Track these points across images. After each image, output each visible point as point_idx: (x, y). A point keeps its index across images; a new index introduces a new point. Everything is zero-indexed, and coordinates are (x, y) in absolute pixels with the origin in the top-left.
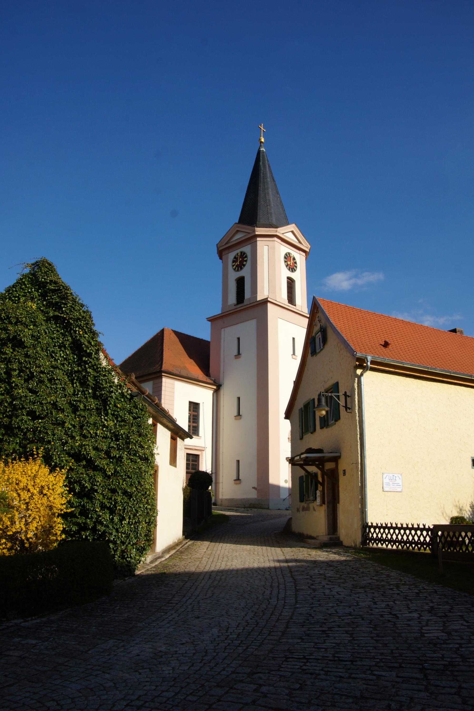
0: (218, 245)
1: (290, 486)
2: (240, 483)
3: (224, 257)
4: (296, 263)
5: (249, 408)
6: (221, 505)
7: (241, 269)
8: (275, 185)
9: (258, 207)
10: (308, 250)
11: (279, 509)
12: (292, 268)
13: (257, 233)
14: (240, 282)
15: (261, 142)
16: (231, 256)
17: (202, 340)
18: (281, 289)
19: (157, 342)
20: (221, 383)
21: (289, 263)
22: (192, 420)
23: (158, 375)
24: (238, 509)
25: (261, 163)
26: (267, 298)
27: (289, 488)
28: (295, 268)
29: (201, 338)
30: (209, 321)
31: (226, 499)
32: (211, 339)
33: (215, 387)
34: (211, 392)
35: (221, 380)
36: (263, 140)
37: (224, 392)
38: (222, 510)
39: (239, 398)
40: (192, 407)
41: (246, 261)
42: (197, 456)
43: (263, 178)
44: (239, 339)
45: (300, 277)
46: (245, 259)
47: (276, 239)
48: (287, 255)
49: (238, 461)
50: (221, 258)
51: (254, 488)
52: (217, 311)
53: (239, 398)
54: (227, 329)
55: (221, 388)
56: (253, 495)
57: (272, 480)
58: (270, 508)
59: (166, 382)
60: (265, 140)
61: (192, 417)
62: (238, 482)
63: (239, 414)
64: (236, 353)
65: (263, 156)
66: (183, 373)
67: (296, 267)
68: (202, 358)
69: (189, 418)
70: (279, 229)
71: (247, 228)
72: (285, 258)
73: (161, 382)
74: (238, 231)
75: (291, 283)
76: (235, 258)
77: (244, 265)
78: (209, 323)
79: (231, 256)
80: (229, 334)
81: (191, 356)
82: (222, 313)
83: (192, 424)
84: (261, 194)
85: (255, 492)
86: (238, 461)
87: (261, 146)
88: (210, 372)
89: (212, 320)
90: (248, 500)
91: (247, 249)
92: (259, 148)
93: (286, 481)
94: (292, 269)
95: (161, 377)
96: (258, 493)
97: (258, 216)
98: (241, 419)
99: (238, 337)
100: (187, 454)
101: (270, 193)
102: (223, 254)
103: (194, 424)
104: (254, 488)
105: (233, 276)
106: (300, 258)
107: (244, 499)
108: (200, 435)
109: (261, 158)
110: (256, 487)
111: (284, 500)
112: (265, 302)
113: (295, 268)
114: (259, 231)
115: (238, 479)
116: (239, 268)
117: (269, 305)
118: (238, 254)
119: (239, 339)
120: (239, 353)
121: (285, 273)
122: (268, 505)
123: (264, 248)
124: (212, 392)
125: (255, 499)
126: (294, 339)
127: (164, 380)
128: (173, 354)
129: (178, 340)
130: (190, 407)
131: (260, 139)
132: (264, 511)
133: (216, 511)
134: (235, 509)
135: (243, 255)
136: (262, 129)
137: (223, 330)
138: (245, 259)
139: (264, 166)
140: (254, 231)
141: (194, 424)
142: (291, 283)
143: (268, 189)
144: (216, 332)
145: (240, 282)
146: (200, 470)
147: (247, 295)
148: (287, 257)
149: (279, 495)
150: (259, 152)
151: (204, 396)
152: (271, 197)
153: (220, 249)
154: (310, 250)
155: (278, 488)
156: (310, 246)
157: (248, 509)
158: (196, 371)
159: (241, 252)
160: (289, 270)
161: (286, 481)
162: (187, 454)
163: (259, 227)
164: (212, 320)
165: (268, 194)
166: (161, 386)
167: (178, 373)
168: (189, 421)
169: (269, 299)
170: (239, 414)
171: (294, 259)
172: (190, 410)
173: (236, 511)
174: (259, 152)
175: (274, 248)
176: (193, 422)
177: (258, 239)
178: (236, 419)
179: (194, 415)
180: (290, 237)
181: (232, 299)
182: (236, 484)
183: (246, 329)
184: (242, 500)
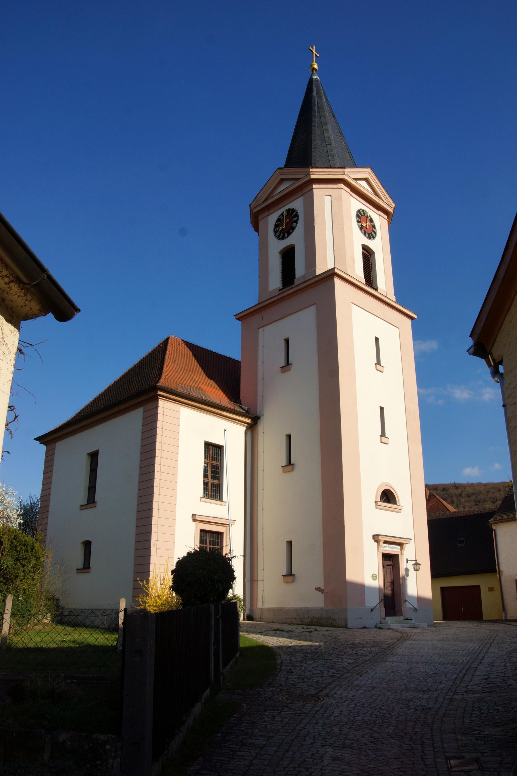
0: (252, 206)
1: (382, 585)
2: (293, 581)
3: (261, 224)
4: (374, 226)
5: (308, 453)
6: (261, 620)
7: (289, 234)
8: (337, 123)
9: (313, 147)
10: (391, 211)
11: (364, 628)
12: (370, 234)
13: (312, 176)
14: (288, 256)
15: (314, 69)
16: (273, 219)
17: (230, 358)
18: (353, 261)
19: (156, 359)
20: (258, 414)
21: (364, 224)
22: (210, 474)
23: (152, 394)
24: (290, 628)
25: (314, 94)
26: (334, 269)
27: (380, 589)
28: (373, 233)
29: (228, 355)
30: (238, 319)
31: (269, 609)
32: (242, 356)
33: (249, 421)
34: (242, 429)
35: (259, 409)
36: (316, 66)
37: (263, 428)
38: (261, 633)
39: (289, 437)
40: (210, 453)
41: (296, 222)
42: (220, 535)
43: (319, 111)
44: (287, 341)
45: (381, 246)
46: (294, 219)
47: (342, 185)
48: (360, 213)
49: (290, 543)
50: (257, 229)
51: (318, 589)
52: (251, 301)
53: (289, 437)
54: (267, 329)
55: (259, 422)
56: (317, 602)
57: (351, 575)
58: (349, 625)
59: (166, 408)
60: (318, 66)
61: (210, 469)
62: (290, 578)
63: (289, 462)
64: (283, 363)
65: (317, 85)
66: (195, 394)
67: (375, 233)
68: (229, 383)
69: (206, 470)
70: (347, 170)
71: (296, 172)
72: (357, 216)
73: (157, 407)
74: (282, 180)
75: (368, 256)
76: (279, 220)
77: (293, 229)
78: (240, 323)
79: (273, 219)
80: (271, 337)
81: (210, 375)
82: (258, 304)
83: (210, 481)
84: (316, 131)
85: (320, 596)
86: (290, 543)
87: (313, 73)
88: (241, 398)
89: (242, 317)
90: (308, 610)
91: (297, 204)
92: (311, 76)
93: (374, 577)
94: (369, 234)
95: (155, 399)
96: (325, 597)
97: (313, 158)
98: (292, 470)
99: (285, 337)
100: (202, 531)
101: (330, 130)
102: (260, 218)
103: (214, 481)
104: (318, 589)
105: (276, 246)
106: (380, 222)
107: (301, 609)
108: (225, 498)
109: (314, 88)
110: (322, 587)
111: (372, 610)
112: (331, 275)
113: (373, 233)
114: (316, 173)
115: (290, 575)
116: (286, 234)
117: (337, 280)
118: (284, 214)
119: (287, 341)
120: (288, 363)
121: (359, 239)
122: (346, 620)
123: (323, 198)
124: (244, 429)
125: (322, 609)
126: (377, 339)
127: (161, 403)
128: (179, 369)
129: (190, 353)
130: (206, 452)
131: (312, 65)
132: (338, 632)
133: (249, 638)
134: (286, 627)
135: (292, 214)
136: (314, 52)
137: (261, 330)
138: (294, 219)
139: (320, 97)
140: (309, 174)
141: (214, 481)
142: (368, 256)
143: (326, 124)
144: (250, 344)
145: (288, 256)
146: (45, 447)
147: (300, 271)
148: (361, 215)
149: (363, 602)
150: (311, 81)
151: (231, 434)
152: (331, 133)
153: (255, 211)
154: (394, 211)
155: (360, 588)
156: (394, 205)
157: (312, 628)
158: (217, 395)
159: (288, 211)
160: (365, 235)
161: (374, 577)
162: (202, 531)
163: (316, 167)
164: (242, 317)
165: (327, 130)
166: (156, 414)
167: (186, 392)
168: (205, 476)
169: (336, 271)
170: (289, 462)
171: (371, 221)
172: (206, 457)
173: (290, 635)
174: (311, 81)
175: (340, 199)
176: (212, 478)
177: (315, 186)
178: (284, 472)
179: (213, 466)
180: (363, 186)
181: (275, 281)
182: (287, 582)
183: (299, 325)
184: (296, 610)
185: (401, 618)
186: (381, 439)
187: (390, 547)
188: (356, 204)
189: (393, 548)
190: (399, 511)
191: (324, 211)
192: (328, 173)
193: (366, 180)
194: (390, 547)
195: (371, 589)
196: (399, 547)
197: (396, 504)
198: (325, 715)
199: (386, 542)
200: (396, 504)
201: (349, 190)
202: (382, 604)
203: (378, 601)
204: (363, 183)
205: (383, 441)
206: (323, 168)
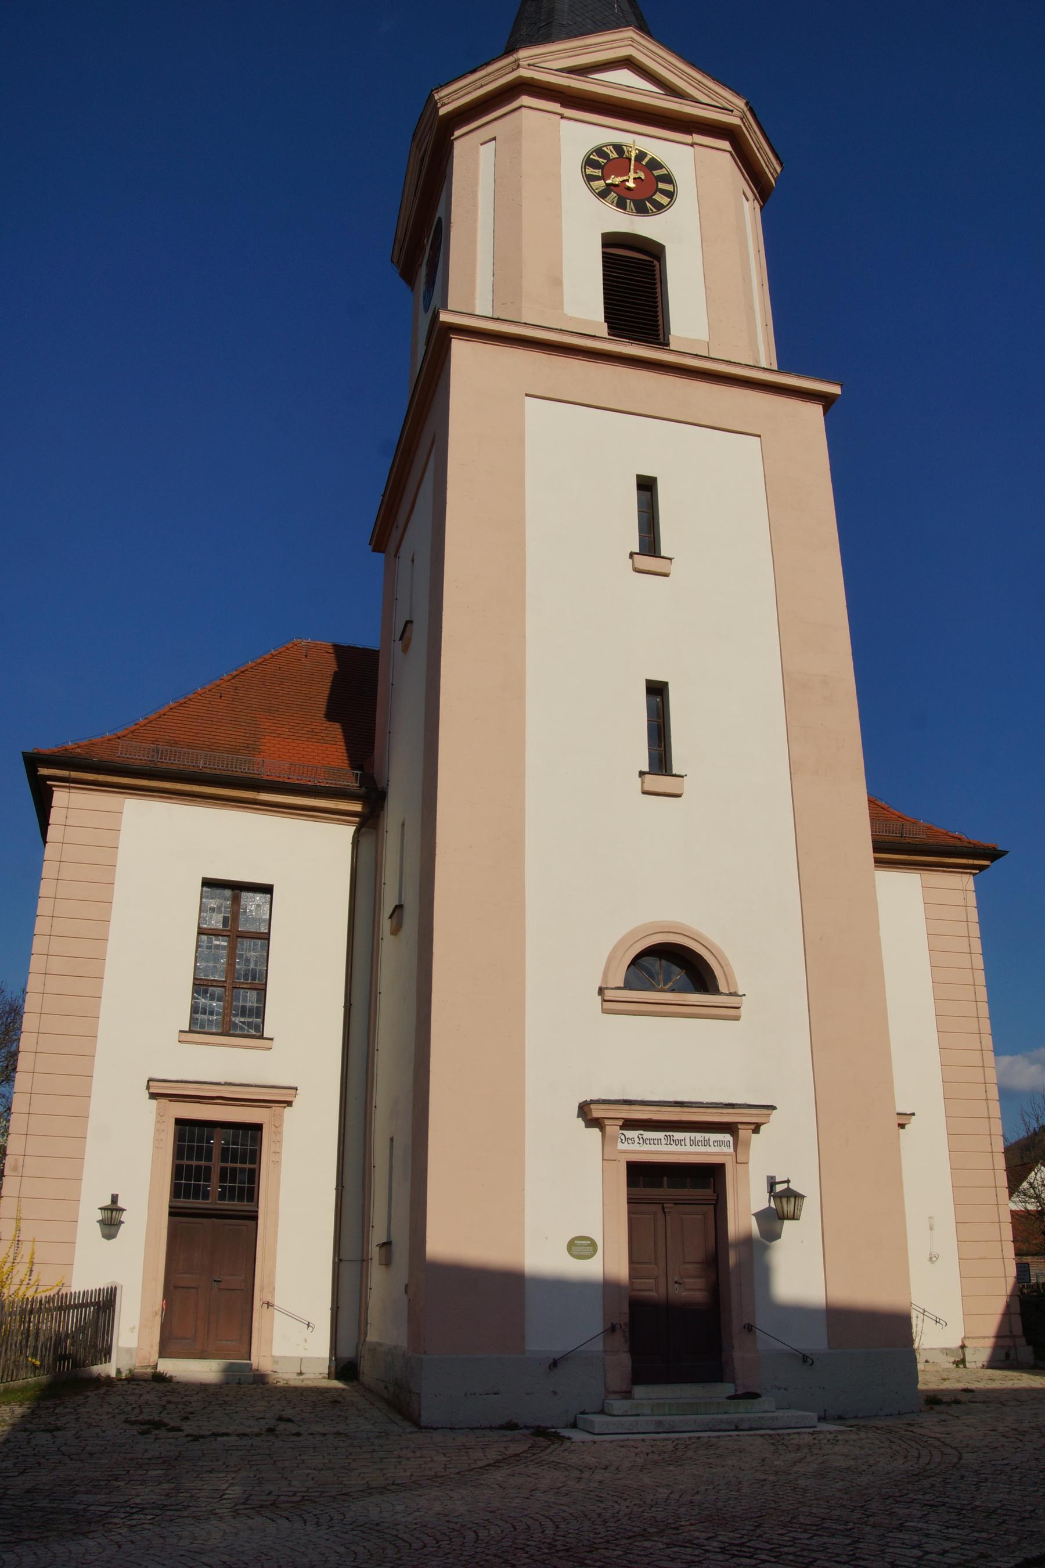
27: (608, 1287)
33: (357, 807)
47: (525, 100)
48: (664, 192)
93: (581, 1247)
111: (555, 1364)
148: (600, 164)
156: (741, 103)
185: (729, 1389)
186: (643, 783)
187: (679, 1142)
188: (582, 135)
189: (693, 1143)
190: (732, 1013)
191: (474, 195)
192: (478, 84)
193: (628, 63)
194: (679, 1142)
195: (559, 1288)
196: (728, 1137)
197: (716, 991)
198: (846, 1497)
199: (629, 1124)
200: (716, 991)
201: (556, 107)
202: (620, 1342)
203: (597, 1326)
204: (624, 77)
205: (647, 788)
206: (463, 76)
